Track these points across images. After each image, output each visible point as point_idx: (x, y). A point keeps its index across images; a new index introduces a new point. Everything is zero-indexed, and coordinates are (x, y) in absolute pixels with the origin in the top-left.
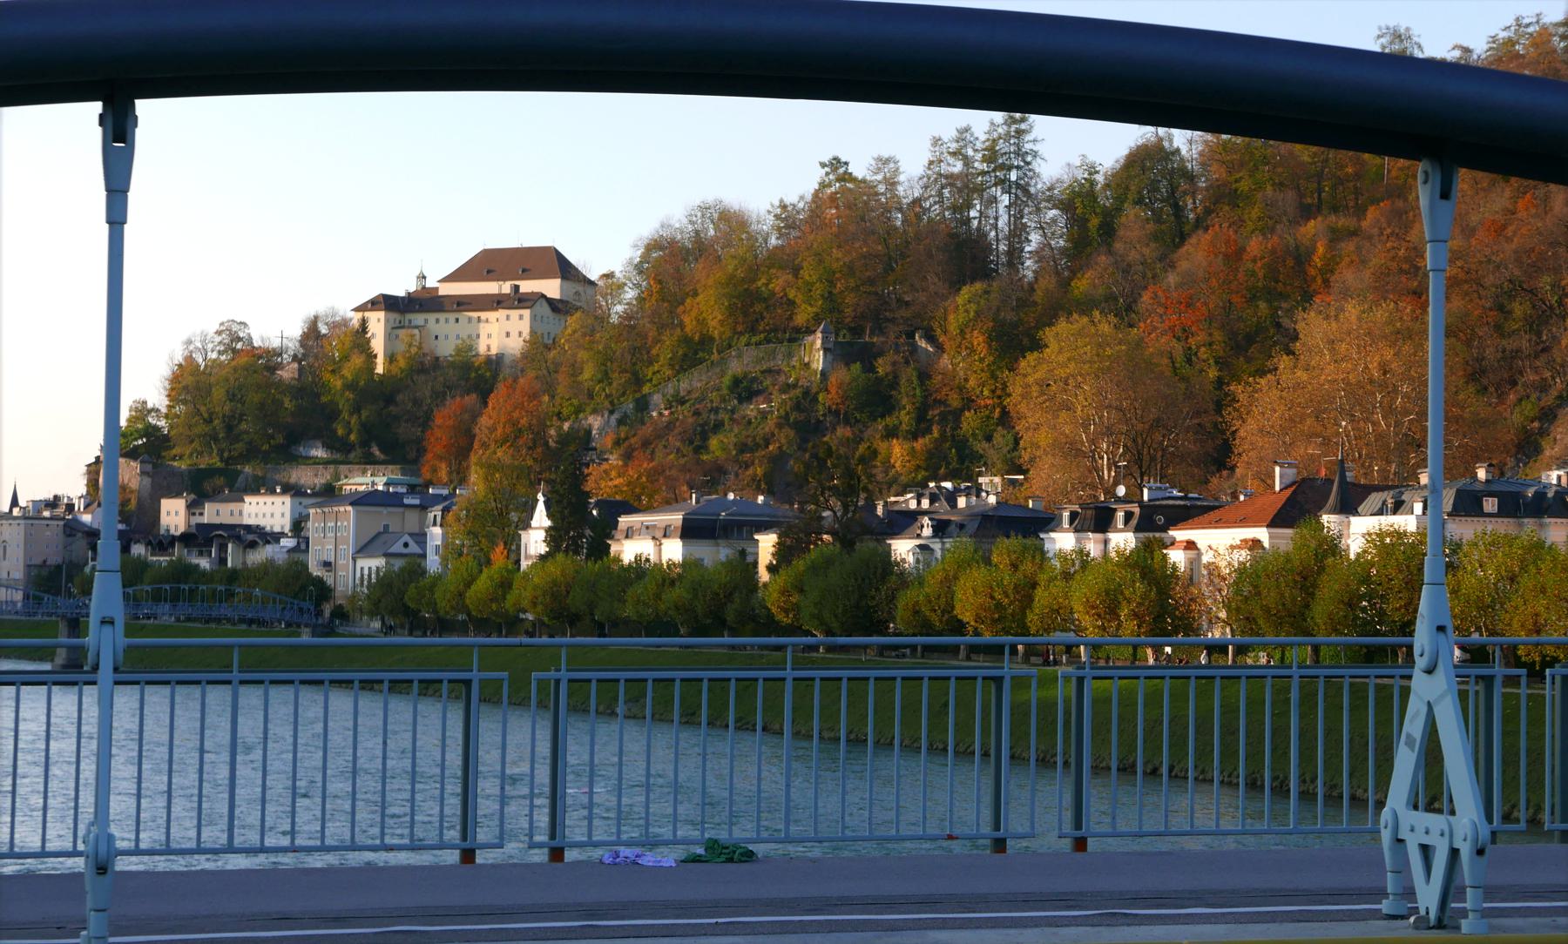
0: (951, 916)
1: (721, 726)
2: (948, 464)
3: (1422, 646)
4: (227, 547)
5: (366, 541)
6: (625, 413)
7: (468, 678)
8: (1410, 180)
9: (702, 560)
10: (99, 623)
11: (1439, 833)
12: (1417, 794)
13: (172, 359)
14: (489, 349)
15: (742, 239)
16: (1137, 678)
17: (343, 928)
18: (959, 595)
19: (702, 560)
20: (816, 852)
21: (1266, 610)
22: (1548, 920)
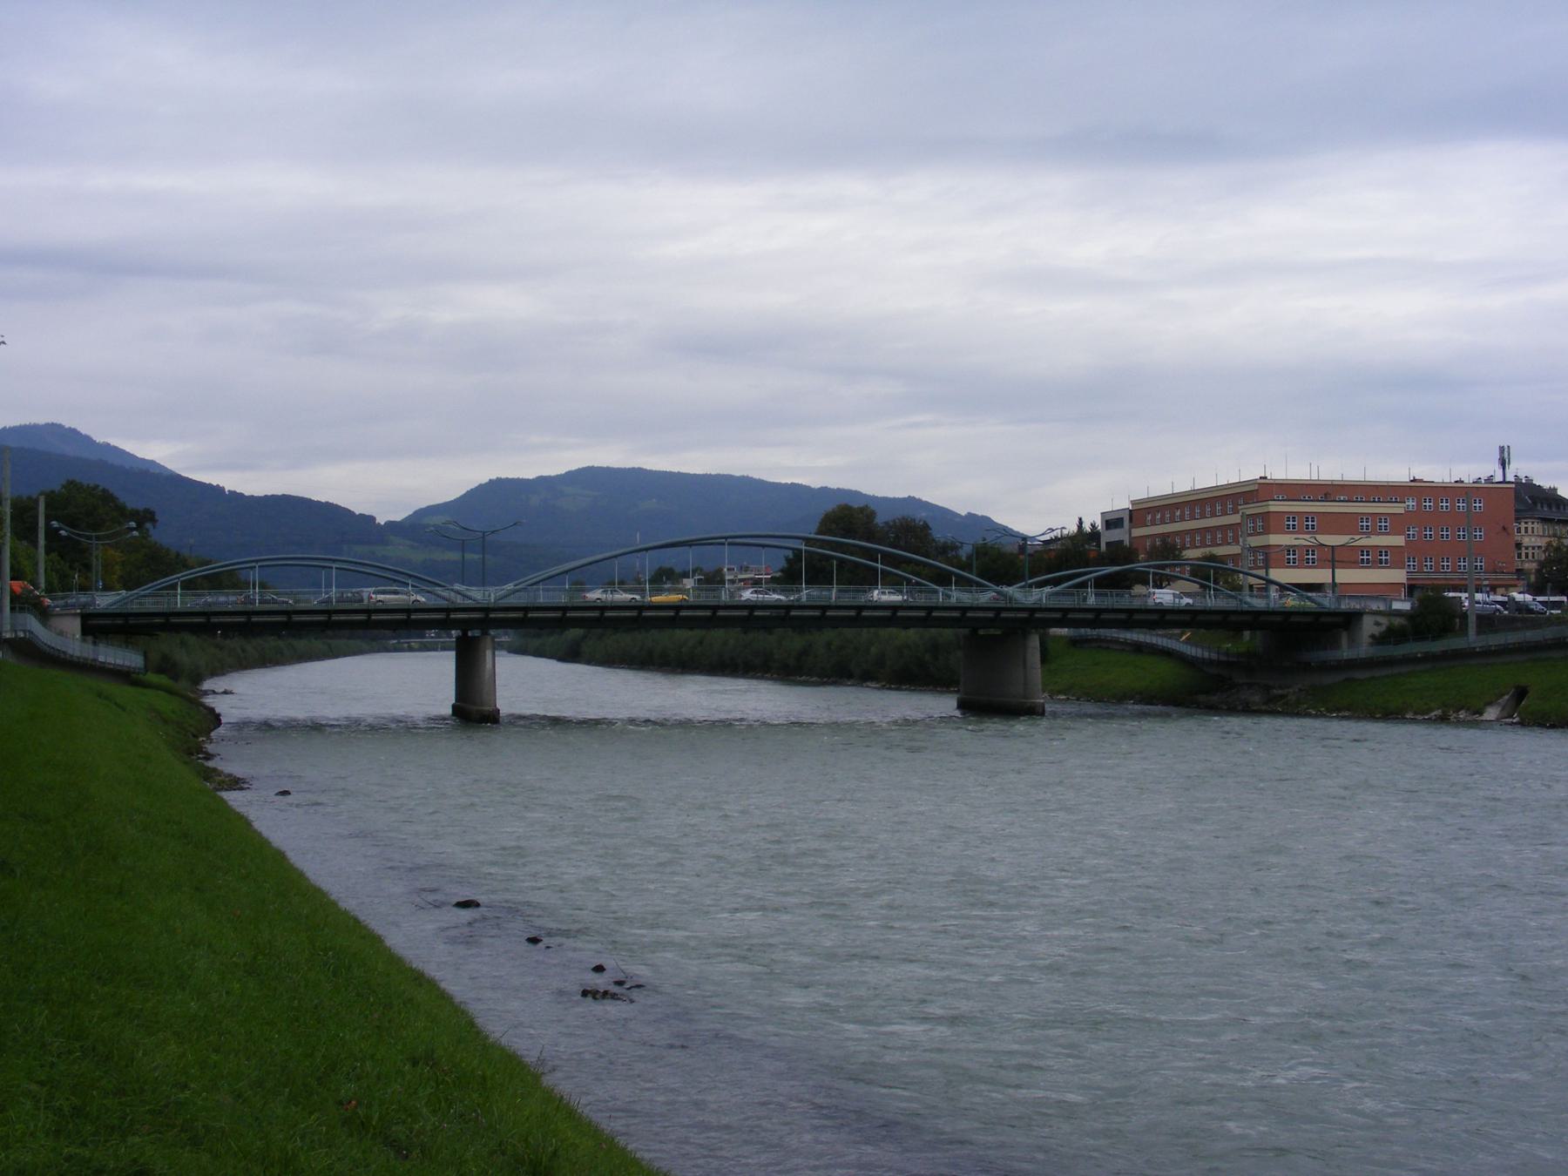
0: (909, 555)
1: (1422, 587)
2: (731, 868)
3: (752, 593)
4: (1558, 610)
5: (1385, 545)
6: (184, 989)
7: (1475, 618)
8: (361, 728)
9: (1123, 541)
10: (482, 735)
11: (531, 946)
12: (738, 690)
13: (442, 981)
14: (236, 783)
15: (339, 1036)
16: (724, 544)
17: (898, 554)
18: (557, 938)
19: (1123, 541)
20: (1304, 1126)
21: (386, 1134)
22: (374, 596)
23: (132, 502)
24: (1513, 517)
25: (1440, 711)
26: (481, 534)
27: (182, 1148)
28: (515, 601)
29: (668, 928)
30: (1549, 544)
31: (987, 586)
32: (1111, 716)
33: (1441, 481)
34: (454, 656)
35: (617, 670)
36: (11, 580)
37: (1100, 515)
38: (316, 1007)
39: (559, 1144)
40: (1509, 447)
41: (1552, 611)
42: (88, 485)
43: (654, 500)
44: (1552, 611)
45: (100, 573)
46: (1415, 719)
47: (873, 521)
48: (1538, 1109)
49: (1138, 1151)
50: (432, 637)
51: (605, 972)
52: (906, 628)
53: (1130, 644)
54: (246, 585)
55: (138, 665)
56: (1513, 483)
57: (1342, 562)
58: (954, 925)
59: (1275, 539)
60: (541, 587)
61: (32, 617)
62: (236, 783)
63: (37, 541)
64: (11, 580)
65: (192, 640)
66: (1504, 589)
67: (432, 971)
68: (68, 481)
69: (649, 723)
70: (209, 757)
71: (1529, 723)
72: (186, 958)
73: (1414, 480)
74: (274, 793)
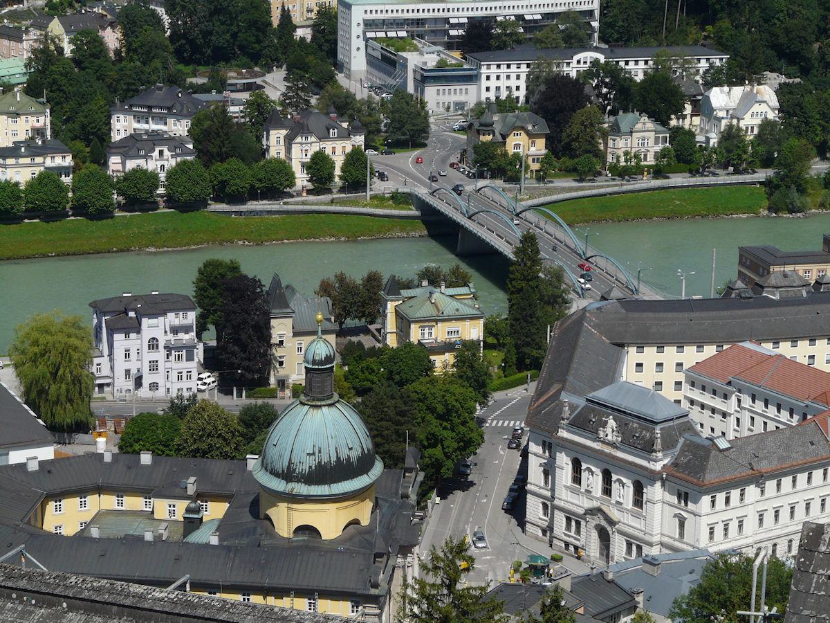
25: (559, 434)
28: (533, 519)
29: (17, 115)
30: (45, 59)
31: (554, 409)
34: (783, 343)
35: (444, 249)
38: (135, 22)
39: (462, 170)
41: (684, 281)
42: (286, 79)
43: (126, 4)
44: (684, 281)
47: (355, 99)
48: (298, 565)
49: (247, 313)
51: (90, 301)
52: (443, 353)
53: (502, 46)
54: (817, 25)
55: (122, 117)
62: (310, 467)
66: (349, 604)
67: (509, 391)
70: (283, 471)
72: (791, 7)
73: (20, 223)
74: (416, 63)
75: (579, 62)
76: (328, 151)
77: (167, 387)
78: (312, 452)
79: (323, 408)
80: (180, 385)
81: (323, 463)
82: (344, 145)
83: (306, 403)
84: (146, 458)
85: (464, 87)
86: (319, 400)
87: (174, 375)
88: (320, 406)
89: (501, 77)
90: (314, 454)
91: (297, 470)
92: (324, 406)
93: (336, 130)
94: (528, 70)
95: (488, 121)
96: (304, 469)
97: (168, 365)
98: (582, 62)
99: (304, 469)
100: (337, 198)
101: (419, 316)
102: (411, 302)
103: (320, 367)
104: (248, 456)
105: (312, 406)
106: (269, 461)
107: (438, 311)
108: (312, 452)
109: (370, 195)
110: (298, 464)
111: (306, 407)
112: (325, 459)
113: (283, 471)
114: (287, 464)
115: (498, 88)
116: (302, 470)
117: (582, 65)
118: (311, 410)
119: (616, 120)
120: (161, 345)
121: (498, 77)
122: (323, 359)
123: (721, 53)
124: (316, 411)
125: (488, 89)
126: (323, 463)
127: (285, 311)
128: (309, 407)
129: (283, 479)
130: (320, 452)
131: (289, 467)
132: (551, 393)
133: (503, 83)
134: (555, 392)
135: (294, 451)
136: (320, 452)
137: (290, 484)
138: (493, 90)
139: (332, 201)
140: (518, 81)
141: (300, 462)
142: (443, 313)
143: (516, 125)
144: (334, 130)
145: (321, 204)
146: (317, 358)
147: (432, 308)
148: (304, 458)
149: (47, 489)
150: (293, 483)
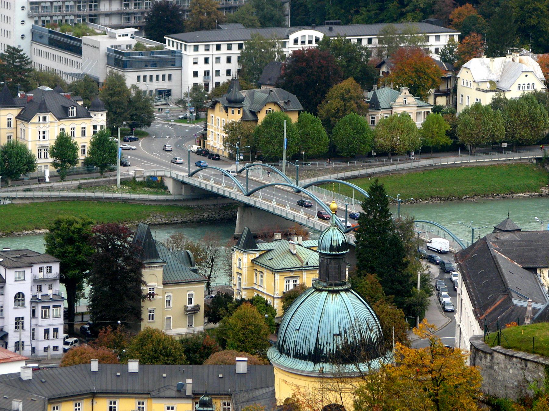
23: (420, 156)
24: (39, 271)
26: (335, 337)
27: (316, 96)
32: (283, 374)
33: (482, 79)
36: (170, 318)
37: (221, 49)
40: (2, 7)
45: (520, 162)
46: (195, 398)
50: (129, 155)
56: (318, 266)
57: (495, 264)
58: (36, 388)
59: (58, 314)
60: (261, 193)
61: (335, 87)
62: (337, 347)
63: (539, 322)
64: (170, 318)
65: (329, 381)
68: (132, 85)
69: (276, 105)
70: (310, 353)
71: (446, 94)
75: (296, 42)
76: (68, 132)
77: (33, 346)
78: (338, 333)
79: (341, 293)
80: (46, 344)
81: (349, 343)
82: (83, 125)
83: (324, 288)
84: (133, 366)
85: (167, 73)
86: (336, 285)
87: (40, 333)
88: (337, 292)
89: (210, 60)
90: (340, 334)
91: (325, 351)
92: (342, 291)
93: (75, 110)
94: (239, 51)
95: (238, 97)
96: (331, 348)
97: (34, 321)
98: (307, 42)
99: (331, 348)
100: (84, 184)
101: (284, 267)
102: (269, 255)
103: (337, 253)
104: (237, 359)
105: (330, 292)
106: (292, 345)
107: (302, 262)
108: (338, 333)
109: (121, 179)
110: (325, 344)
111: (324, 294)
112: (351, 340)
113: (310, 353)
114: (314, 345)
115: (207, 73)
116: (330, 350)
117: (307, 45)
118: (330, 296)
119: (375, 95)
120: (28, 298)
121: (207, 61)
122: (340, 245)
123: (449, 30)
124: (334, 296)
125: (195, 74)
126: (349, 343)
127: (155, 260)
128: (327, 292)
129: (309, 361)
130: (345, 332)
131: (316, 349)
132: (498, 304)
133: (201, 68)
134: (502, 302)
135: (320, 333)
136: (345, 332)
137: (318, 365)
138: (201, 74)
139: (79, 188)
140: (195, 78)
141: (327, 343)
142: (307, 264)
143: (268, 101)
144: (72, 108)
145: (63, 190)
146: (335, 244)
147: (294, 259)
148: (330, 339)
149: (46, 395)
150: (321, 364)
